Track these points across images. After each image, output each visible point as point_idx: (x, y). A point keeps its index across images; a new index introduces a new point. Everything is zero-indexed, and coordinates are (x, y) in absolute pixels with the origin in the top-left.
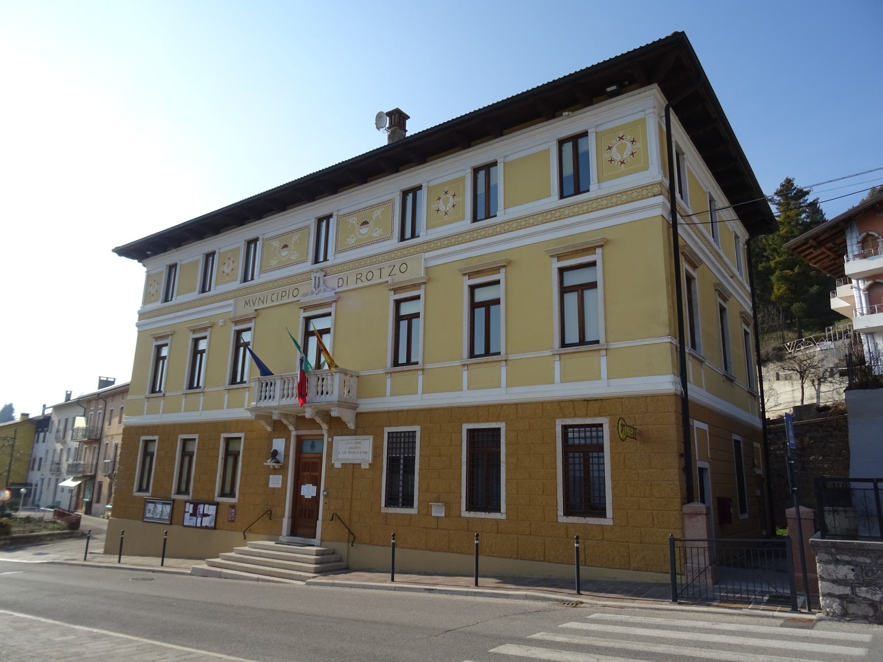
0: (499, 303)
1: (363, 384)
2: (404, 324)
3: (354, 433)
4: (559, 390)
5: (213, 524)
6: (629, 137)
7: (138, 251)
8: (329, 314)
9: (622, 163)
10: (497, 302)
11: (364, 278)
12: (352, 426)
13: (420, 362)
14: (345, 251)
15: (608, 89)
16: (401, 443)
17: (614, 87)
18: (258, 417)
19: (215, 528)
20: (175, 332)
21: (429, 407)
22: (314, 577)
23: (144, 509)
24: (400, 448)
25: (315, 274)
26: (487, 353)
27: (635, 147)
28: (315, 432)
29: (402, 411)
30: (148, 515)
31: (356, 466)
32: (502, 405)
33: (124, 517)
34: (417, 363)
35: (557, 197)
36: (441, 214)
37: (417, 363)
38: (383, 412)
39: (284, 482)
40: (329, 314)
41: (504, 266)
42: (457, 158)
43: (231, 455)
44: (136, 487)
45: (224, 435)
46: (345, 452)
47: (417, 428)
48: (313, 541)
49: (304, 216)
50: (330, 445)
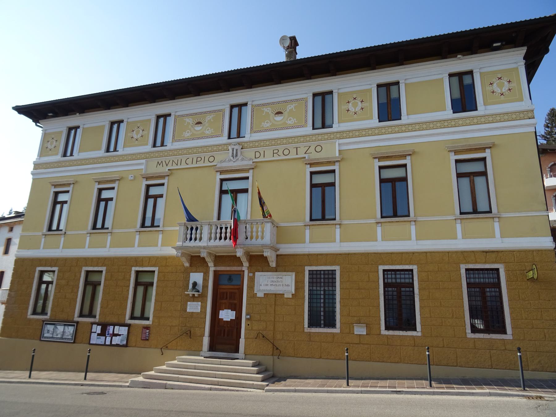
0: (162, 197)
1: (281, 234)
2: (103, 204)
3: (276, 270)
4: (460, 243)
5: (125, 343)
6: (505, 79)
7: (36, 112)
8: (68, 192)
9: (502, 94)
10: (111, 199)
11: (280, 153)
12: (273, 264)
13: (110, 228)
14: (179, 141)
15: (495, 45)
16: (321, 278)
17: (499, 44)
18: (183, 254)
19: (126, 346)
20: (77, 182)
21: (348, 252)
22: (267, 385)
23: (42, 330)
24: (321, 282)
25: (233, 147)
26: (152, 225)
27: (363, 105)
28: (239, 268)
29: (321, 255)
30: (46, 335)
31: (278, 297)
32: (413, 253)
33: (17, 337)
34: (108, 228)
35: (227, 138)
36: (134, 140)
37: (108, 228)
38: (304, 255)
39: (204, 308)
40: (68, 192)
41: (410, 155)
42: (325, 81)
43: (92, 285)
44: (30, 310)
45: (134, 269)
46: (267, 285)
47: (337, 268)
48: (236, 355)
49: (222, 102)
50: (252, 280)
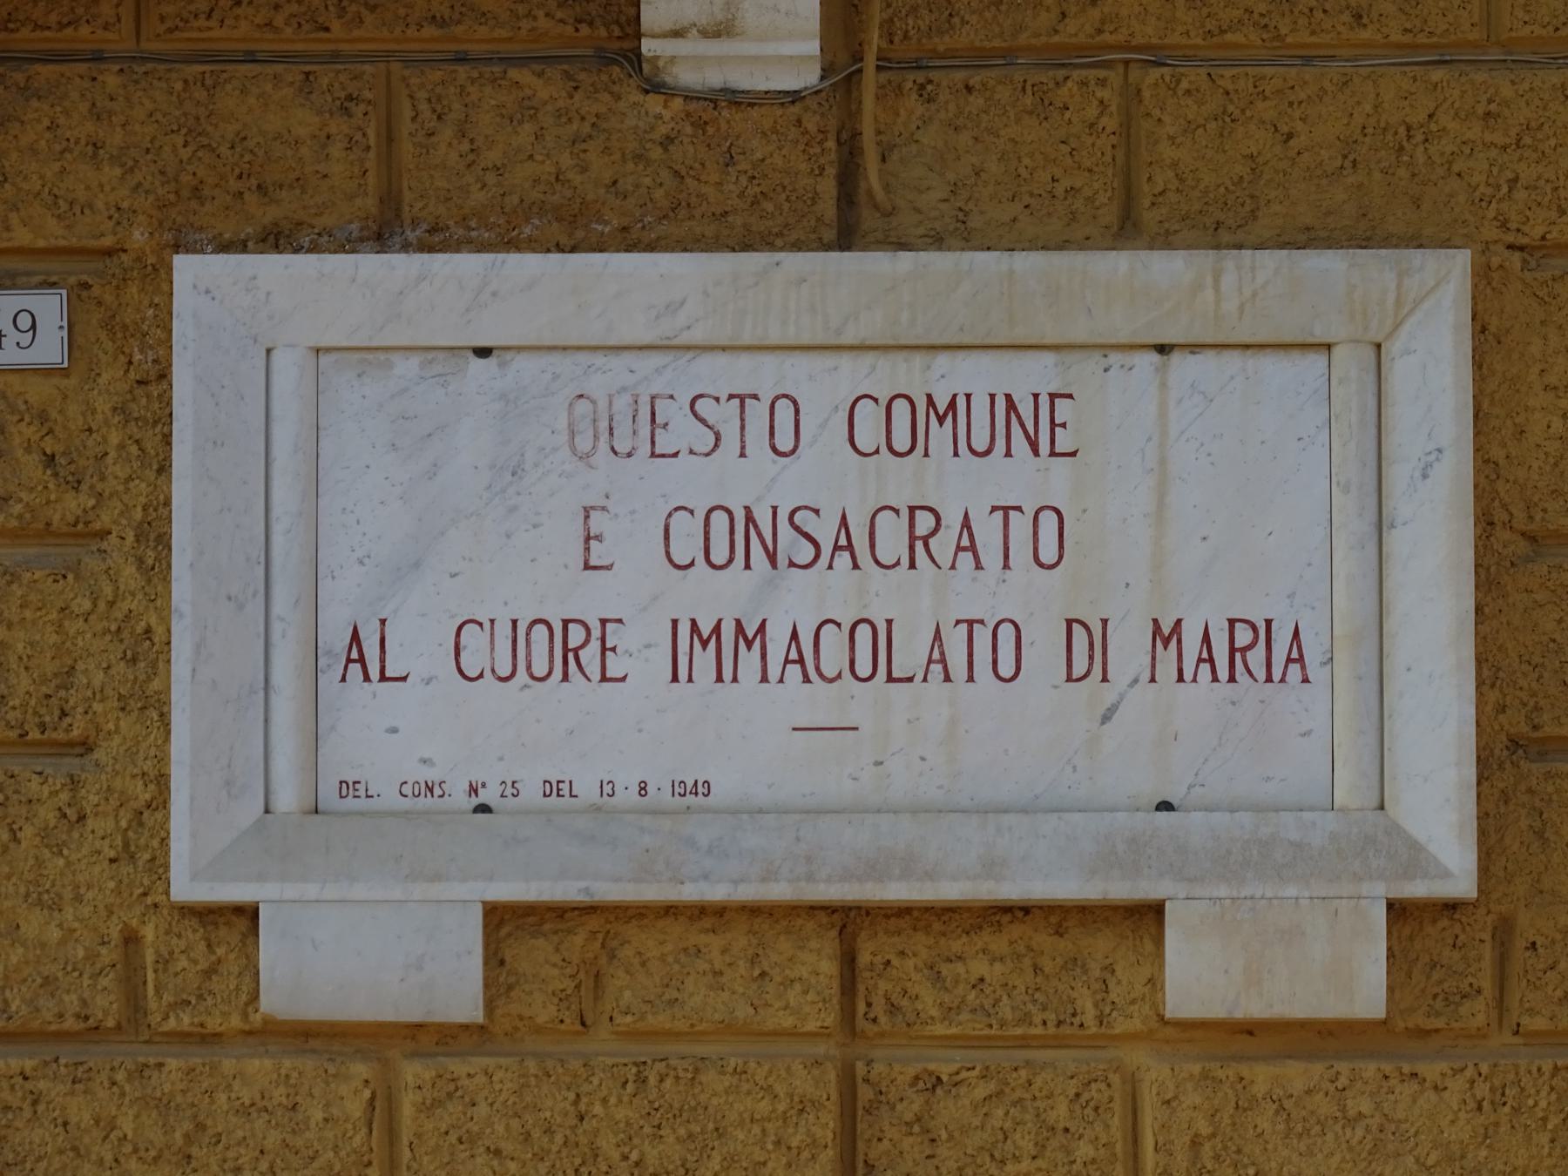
46: (574, 649)
